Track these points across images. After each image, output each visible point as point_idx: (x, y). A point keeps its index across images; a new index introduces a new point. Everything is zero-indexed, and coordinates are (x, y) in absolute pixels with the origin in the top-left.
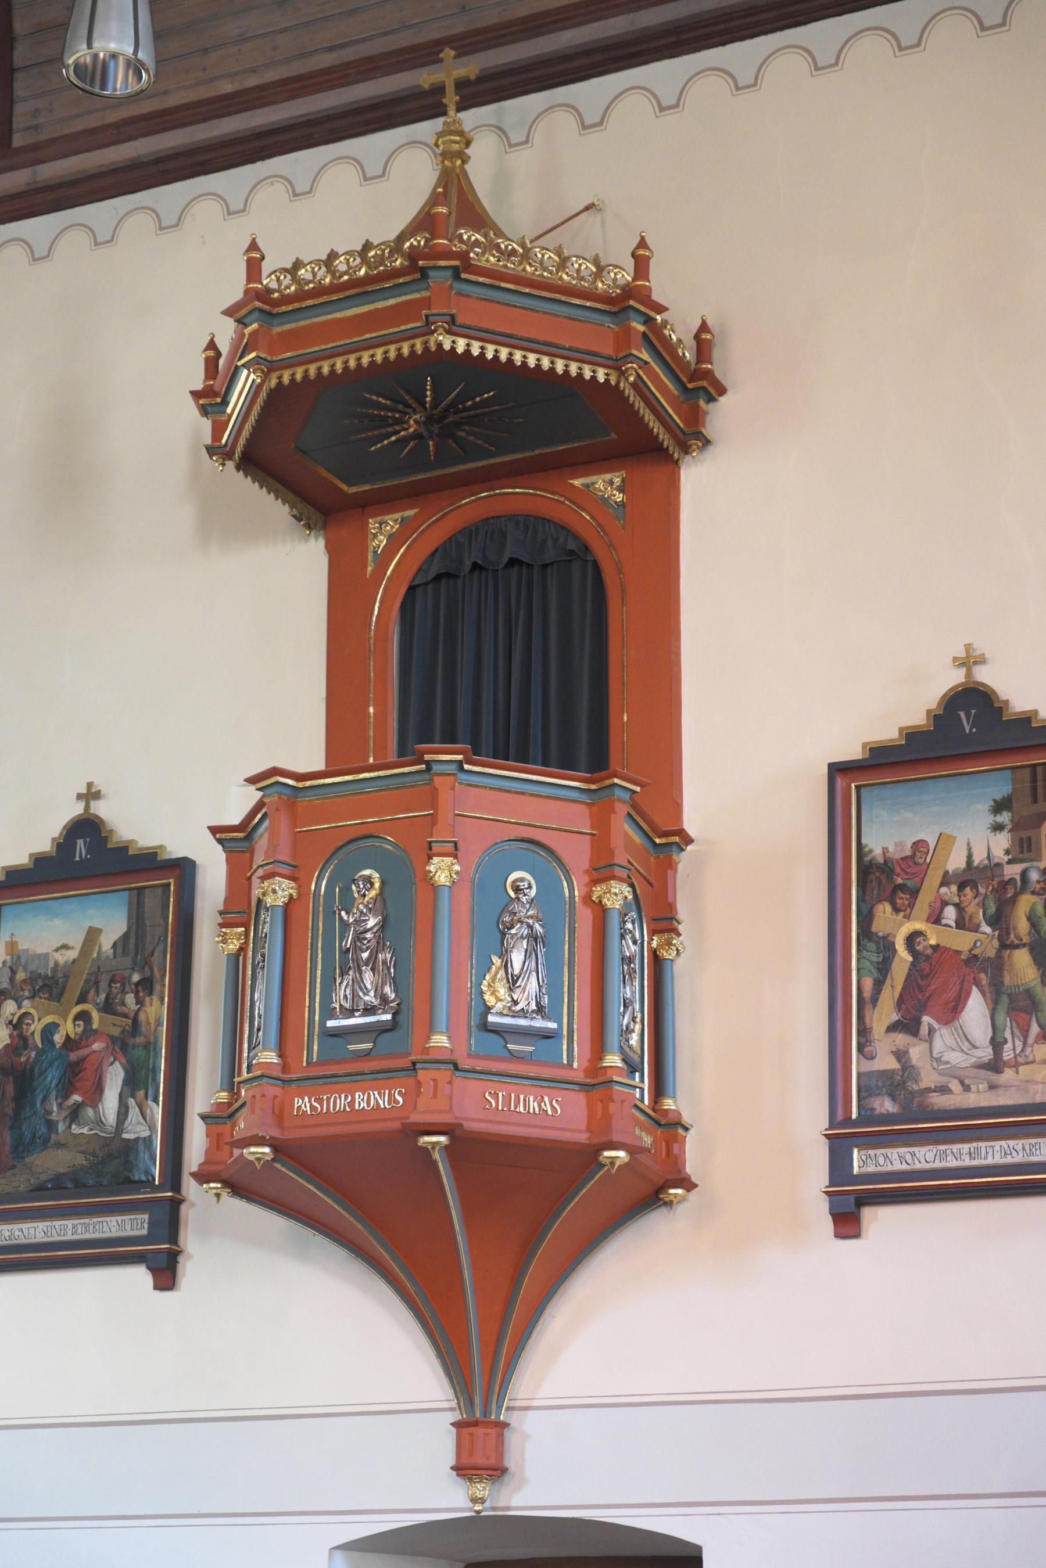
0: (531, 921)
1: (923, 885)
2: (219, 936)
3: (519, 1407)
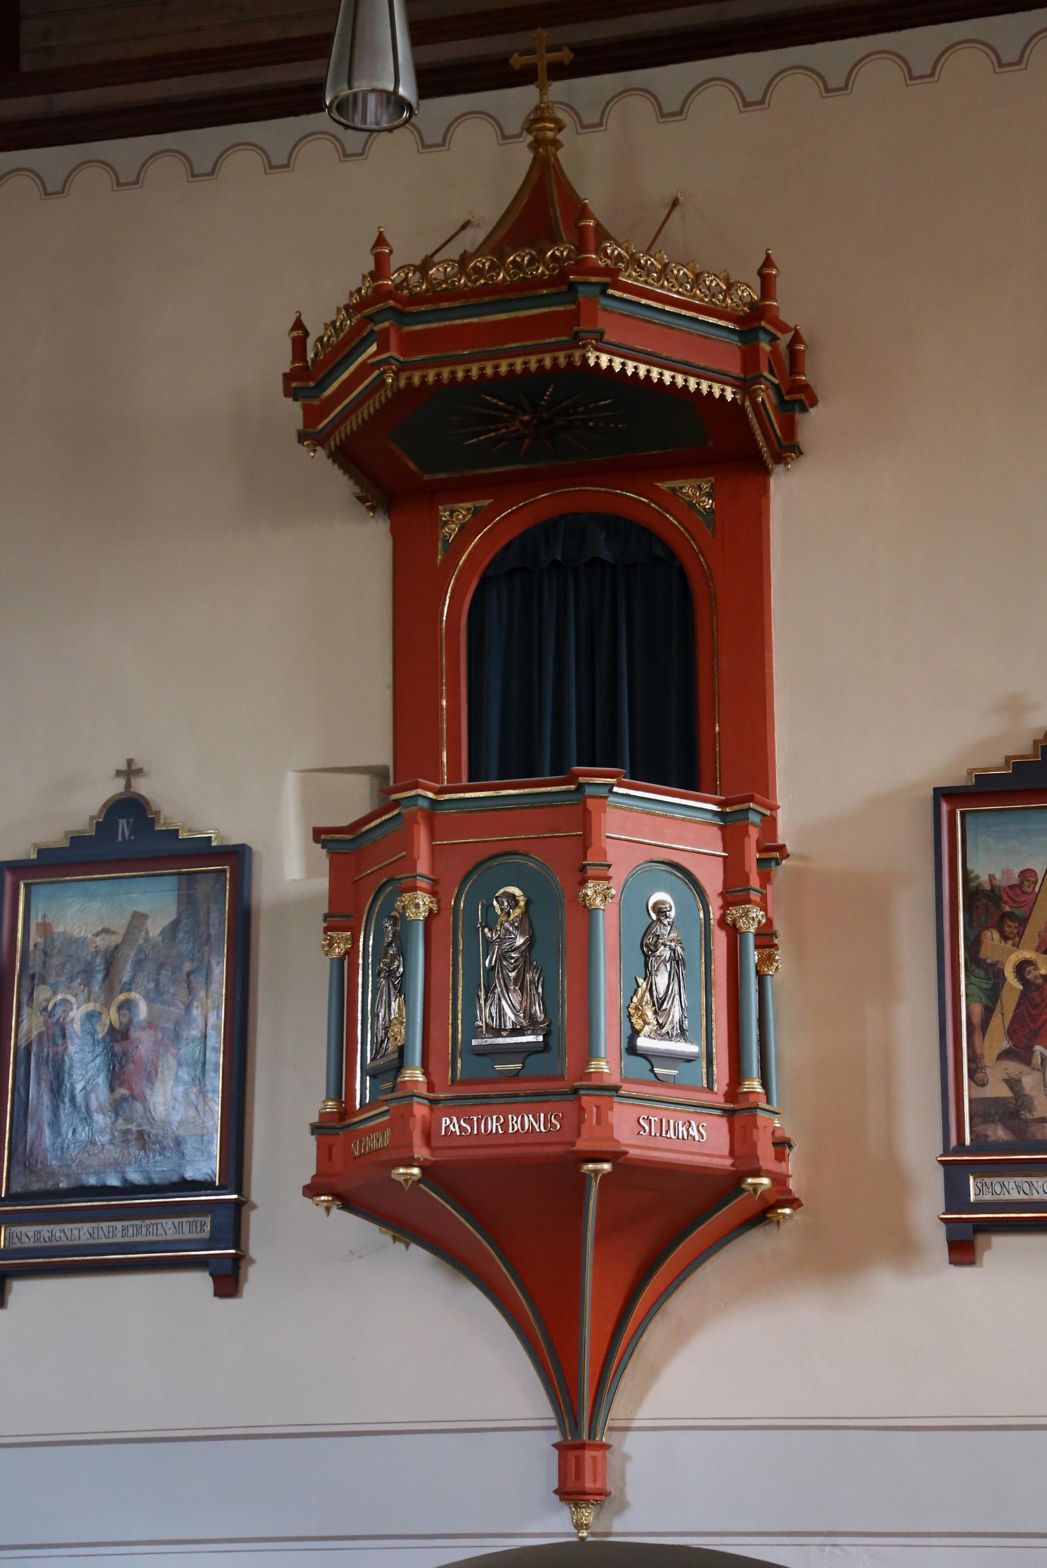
0: (673, 944)
1: (1032, 915)
2: (326, 940)
3: (618, 1427)
